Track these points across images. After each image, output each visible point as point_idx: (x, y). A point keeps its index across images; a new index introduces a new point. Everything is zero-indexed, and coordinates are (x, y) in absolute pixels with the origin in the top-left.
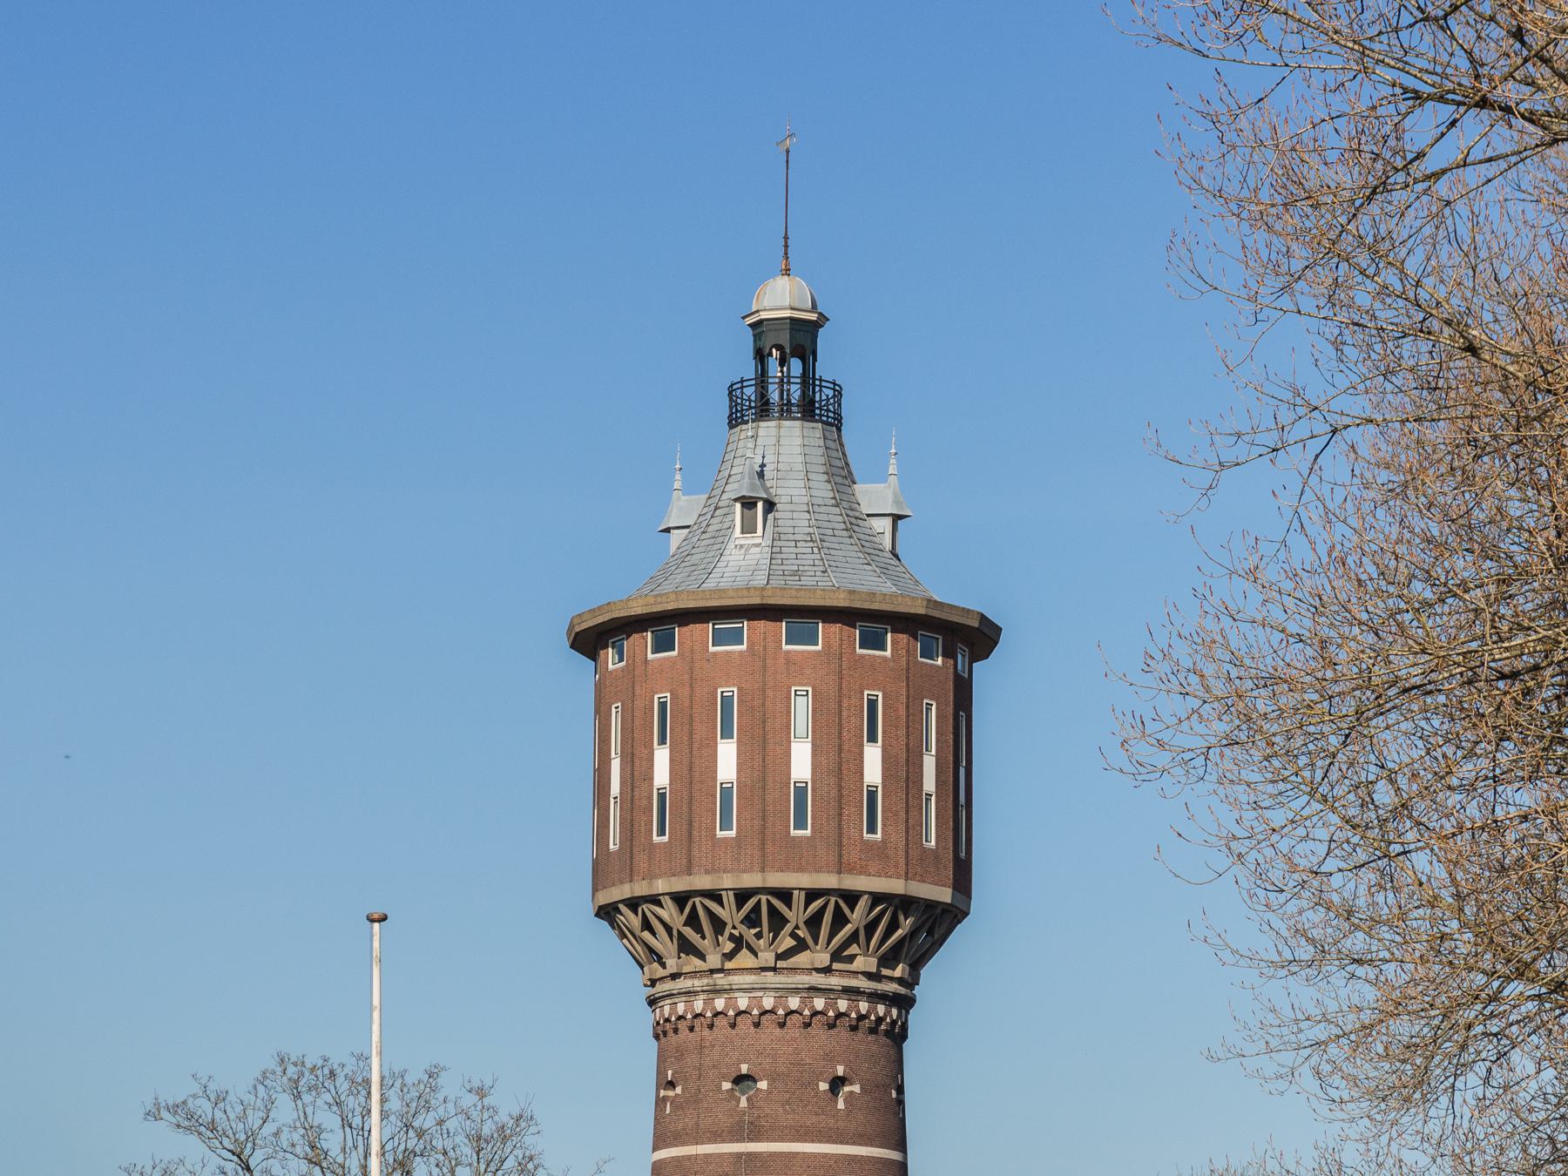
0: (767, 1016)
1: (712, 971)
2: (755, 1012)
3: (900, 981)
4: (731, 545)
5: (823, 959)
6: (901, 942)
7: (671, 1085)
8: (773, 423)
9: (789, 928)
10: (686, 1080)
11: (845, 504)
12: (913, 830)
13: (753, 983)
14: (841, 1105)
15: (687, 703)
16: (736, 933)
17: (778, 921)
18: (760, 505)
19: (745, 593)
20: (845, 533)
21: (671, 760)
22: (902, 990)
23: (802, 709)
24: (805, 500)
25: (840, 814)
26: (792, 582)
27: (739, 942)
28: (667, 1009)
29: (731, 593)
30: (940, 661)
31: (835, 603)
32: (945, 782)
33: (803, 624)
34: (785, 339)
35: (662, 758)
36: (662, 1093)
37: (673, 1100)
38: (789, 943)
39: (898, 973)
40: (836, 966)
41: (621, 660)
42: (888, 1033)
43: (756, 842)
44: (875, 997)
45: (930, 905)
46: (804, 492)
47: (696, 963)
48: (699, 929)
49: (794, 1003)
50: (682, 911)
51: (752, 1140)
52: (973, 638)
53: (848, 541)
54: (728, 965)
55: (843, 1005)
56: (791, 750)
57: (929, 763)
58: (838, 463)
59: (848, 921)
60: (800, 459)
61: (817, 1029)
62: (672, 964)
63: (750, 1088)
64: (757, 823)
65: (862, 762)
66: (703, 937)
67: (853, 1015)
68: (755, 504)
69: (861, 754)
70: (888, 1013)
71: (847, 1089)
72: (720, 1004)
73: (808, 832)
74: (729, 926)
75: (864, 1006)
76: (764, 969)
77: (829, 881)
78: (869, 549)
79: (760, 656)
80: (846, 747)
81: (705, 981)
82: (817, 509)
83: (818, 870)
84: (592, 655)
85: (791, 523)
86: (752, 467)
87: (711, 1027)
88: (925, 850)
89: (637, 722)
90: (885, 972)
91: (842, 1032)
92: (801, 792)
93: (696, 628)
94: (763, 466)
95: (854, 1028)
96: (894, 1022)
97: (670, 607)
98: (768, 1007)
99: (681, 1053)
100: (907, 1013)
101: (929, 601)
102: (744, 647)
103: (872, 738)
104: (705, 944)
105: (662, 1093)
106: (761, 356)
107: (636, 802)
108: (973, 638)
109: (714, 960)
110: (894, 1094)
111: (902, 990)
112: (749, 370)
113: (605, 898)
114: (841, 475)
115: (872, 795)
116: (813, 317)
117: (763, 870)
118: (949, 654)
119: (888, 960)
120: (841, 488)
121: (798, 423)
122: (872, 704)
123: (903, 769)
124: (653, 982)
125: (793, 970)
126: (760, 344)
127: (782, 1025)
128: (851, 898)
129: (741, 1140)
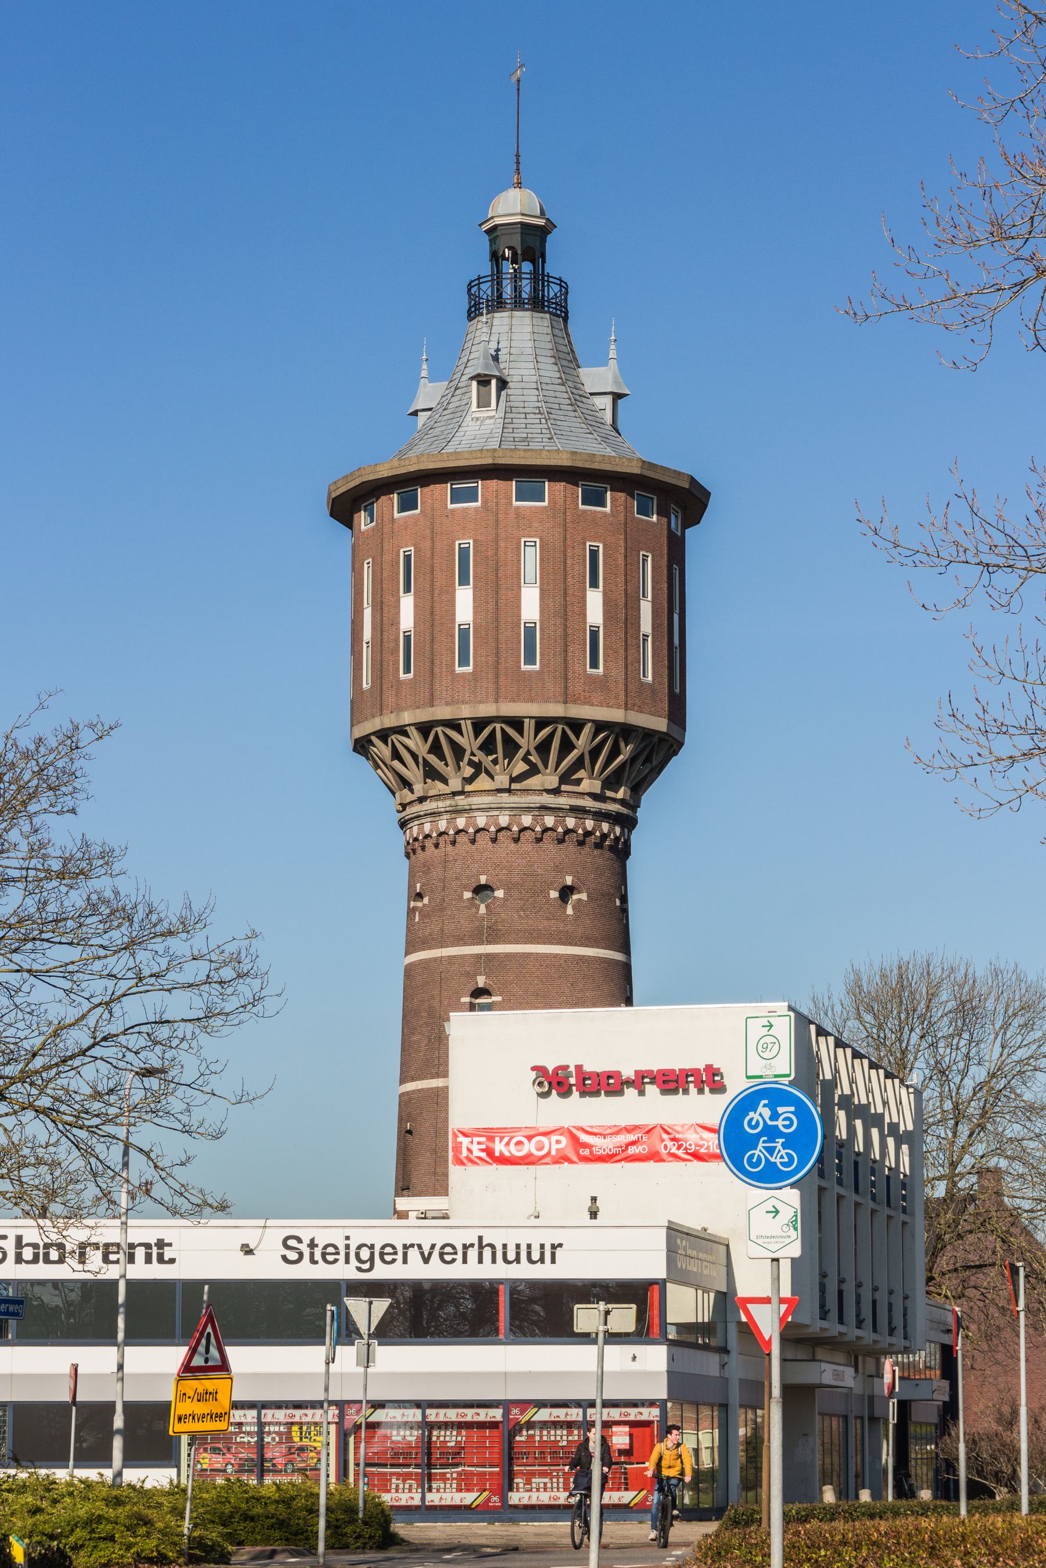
0: (503, 833)
1: (454, 794)
2: (493, 829)
3: (622, 802)
4: (468, 418)
5: (552, 781)
7: (419, 896)
9: (521, 753)
11: (570, 384)
12: (631, 665)
13: (491, 803)
14: (570, 911)
15: (428, 555)
16: (475, 759)
17: (511, 748)
18: (494, 382)
20: (570, 408)
22: (625, 811)
23: (531, 560)
24: (534, 379)
25: (566, 651)
26: (521, 446)
27: (478, 768)
28: (415, 829)
29: (467, 456)
30: (655, 518)
31: (559, 463)
32: (660, 625)
33: (530, 484)
34: (516, 241)
35: (407, 604)
36: (412, 904)
37: (421, 910)
38: (521, 767)
39: (620, 795)
40: (564, 788)
41: (372, 521)
42: (613, 849)
43: (491, 676)
44: (600, 816)
45: (648, 734)
46: (533, 372)
47: (439, 787)
48: (442, 757)
49: (527, 820)
50: (426, 740)
51: (489, 943)
53: (573, 414)
54: (468, 788)
55: (571, 822)
56: (527, 590)
58: (564, 349)
59: (574, 747)
60: (530, 344)
62: (419, 789)
63: (489, 897)
64: (491, 659)
65: (585, 604)
66: (447, 765)
68: (489, 383)
71: (575, 897)
72: (461, 822)
73: (537, 667)
74: (468, 753)
75: (589, 824)
76: (499, 791)
77: (555, 710)
78: (591, 421)
80: (570, 592)
81: (448, 802)
82: (544, 386)
83: (547, 701)
84: (349, 523)
85: (522, 398)
86: (486, 350)
87: (454, 843)
88: (642, 684)
90: (609, 794)
91: (570, 846)
92: (530, 632)
93: (436, 489)
94: (498, 350)
97: (412, 469)
99: (427, 868)
100: (630, 832)
102: (479, 504)
103: (594, 584)
104: (448, 771)
105: (412, 904)
106: (496, 257)
109: (455, 784)
110: (618, 903)
111: (625, 811)
112: (485, 268)
113: (360, 731)
114: (568, 360)
115: (594, 634)
116: (541, 222)
117: (497, 701)
118: (663, 512)
120: (567, 370)
121: (528, 314)
122: (594, 554)
123: (622, 611)
124: (404, 806)
125: (526, 791)
126: (495, 247)
127: (516, 840)
128: (576, 725)
129: (481, 943)
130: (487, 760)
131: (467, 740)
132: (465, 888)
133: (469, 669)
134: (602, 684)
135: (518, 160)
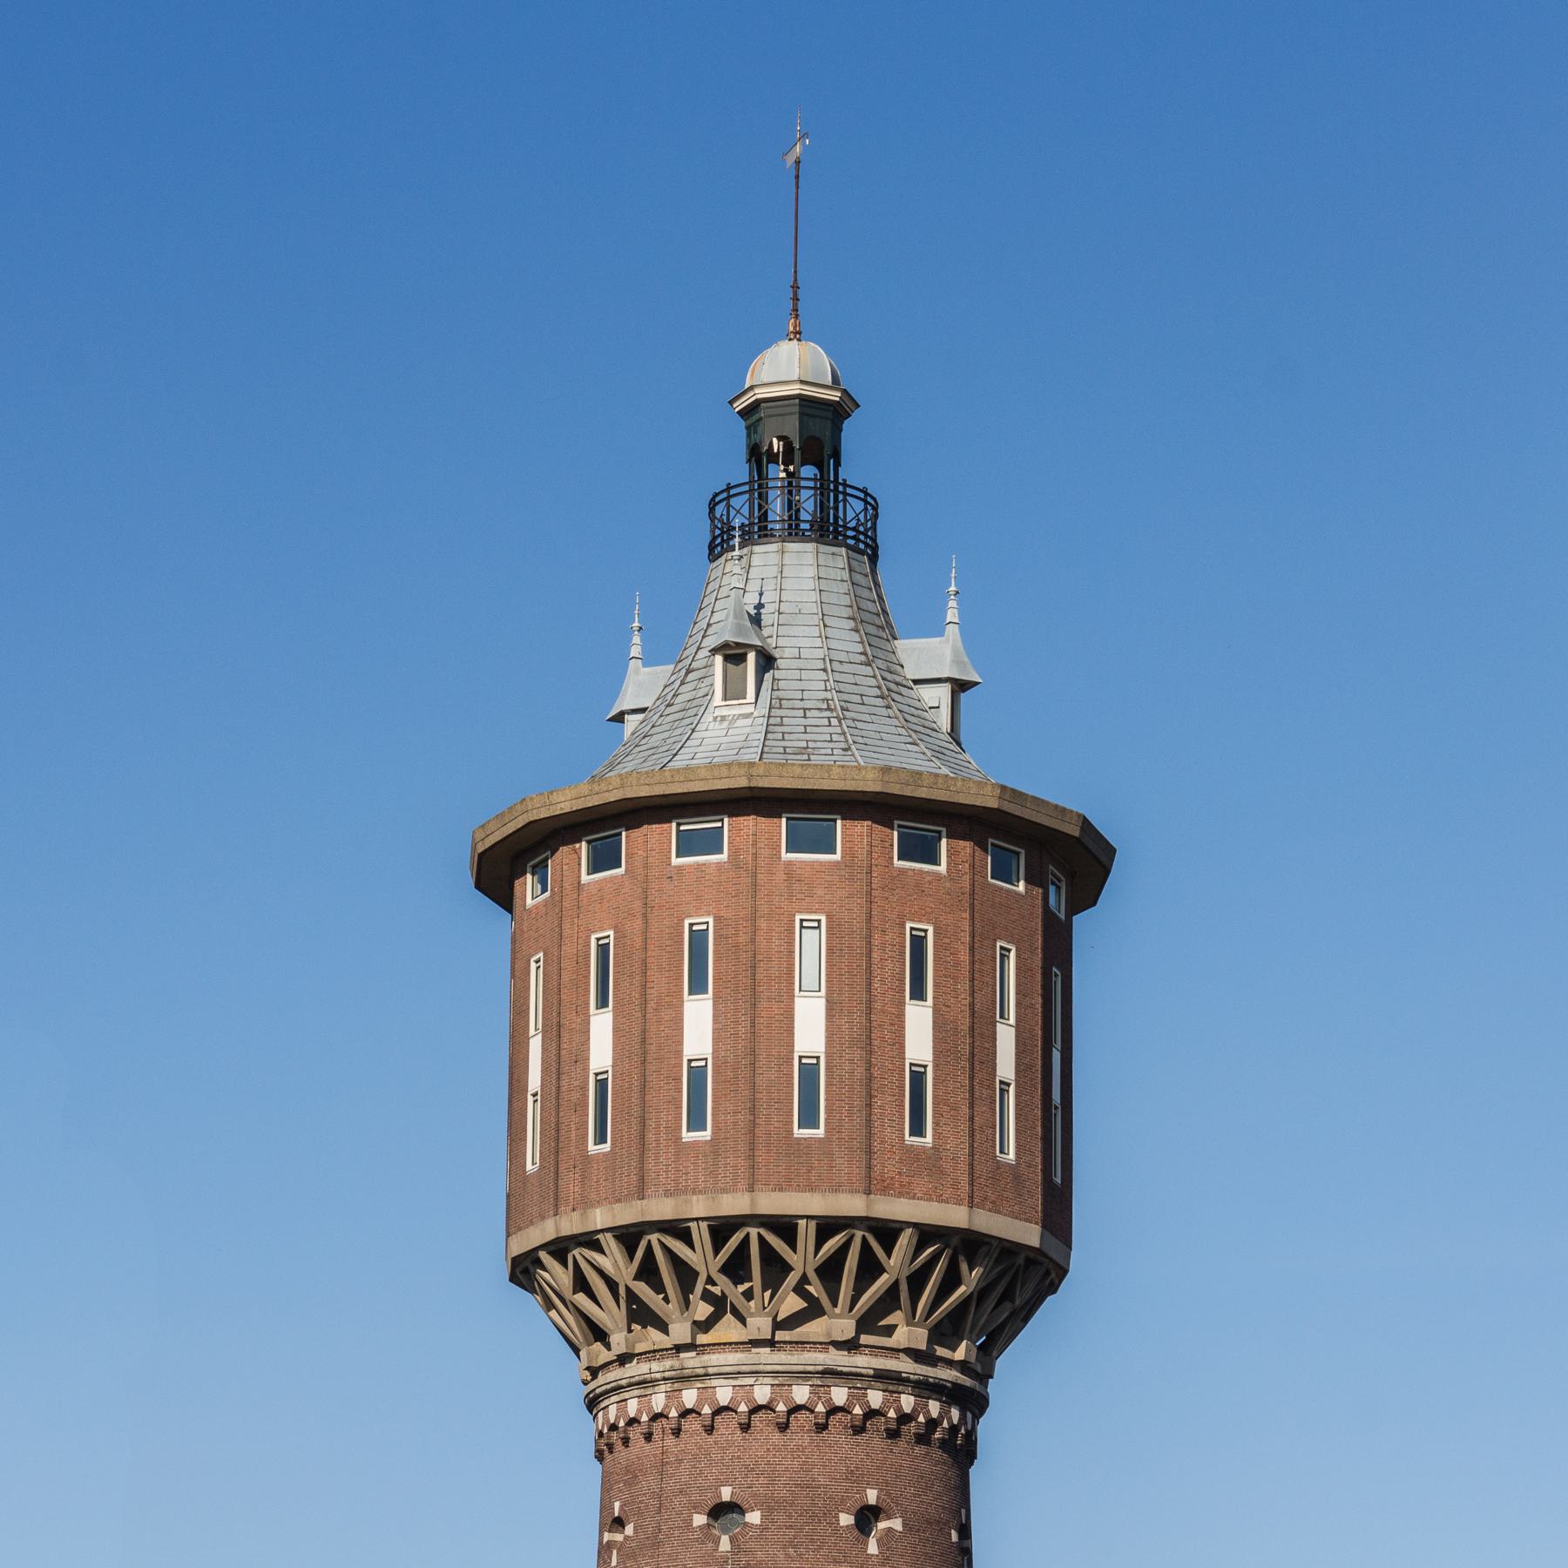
0: (761, 1414)
1: (679, 1348)
2: (743, 1408)
3: (963, 1366)
4: (708, 718)
5: (844, 1327)
6: (964, 1304)
8: (773, 547)
9: (792, 1279)
10: (640, 1514)
12: (980, 1133)
13: (740, 1364)
14: (873, 1548)
15: (638, 942)
16: (716, 1290)
18: (751, 657)
19: (725, 772)
20: (879, 702)
21: (616, 1030)
22: (967, 1382)
23: (811, 950)
24: (820, 653)
25: (869, 1105)
28: (613, 1410)
29: (703, 773)
30: (1021, 887)
32: (1030, 1067)
33: (811, 823)
34: (792, 427)
35: (602, 1026)
36: (607, 1537)
37: (620, 1547)
39: (960, 1354)
40: (865, 1339)
41: (544, 890)
42: (945, 1445)
44: (925, 1388)
45: (1008, 1249)
46: (818, 642)
47: (654, 1337)
48: (659, 1287)
49: (801, 1394)
50: (631, 1258)
52: (1069, 862)
53: (885, 712)
54: (702, 1339)
55: (875, 1398)
56: (797, 1010)
57: (1005, 1038)
58: (870, 606)
59: (882, 1270)
60: (814, 596)
61: (837, 1434)
64: (743, 1118)
67: (892, 1414)
69: (901, 1016)
70: (944, 1414)
71: (882, 1525)
72: (689, 1397)
73: (820, 1132)
75: (907, 1402)
76: (755, 1343)
77: (851, 1205)
78: (916, 724)
79: (748, 870)
80: (877, 1005)
81: (668, 1363)
82: (836, 666)
83: (836, 1189)
84: (505, 898)
86: (739, 605)
87: (677, 1432)
88: (999, 1165)
89: (565, 978)
90: (941, 1352)
91: (874, 1439)
92: (809, 1073)
94: (760, 606)
95: (893, 1434)
96: (954, 1429)
98: (762, 1401)
99: (632, 1475)
101: (1003, 788)
102: (724, 857)
103: (918, 993)
104: (668, 1309)
105: (607, 1537)
106: (758, 456)
107: (564, 1095)
108: (1069, 862)
109: (680, 1331)
110: (954, 1537)
111: (967, 1382)
112: (740, 472)
113: (520, 1245)
114: (877, 626)
115: (918, 1079)
116: (834, 396)
117: (751, 1189)
119: (946, 1332)
120: (874, 641)
121: (810, 546)
122: (918, 943)
123: (966, 1043)
124: (594, 1372)
125: (800, 1344)
126: (755, 438)
127: (783, 1427)
128: (887, 1232)
130: (735, 1292)
131: (703, 1258)
132: (696, 1508)
133: (706, 1135)
134: (930, 1162)
135: (795, 294)
